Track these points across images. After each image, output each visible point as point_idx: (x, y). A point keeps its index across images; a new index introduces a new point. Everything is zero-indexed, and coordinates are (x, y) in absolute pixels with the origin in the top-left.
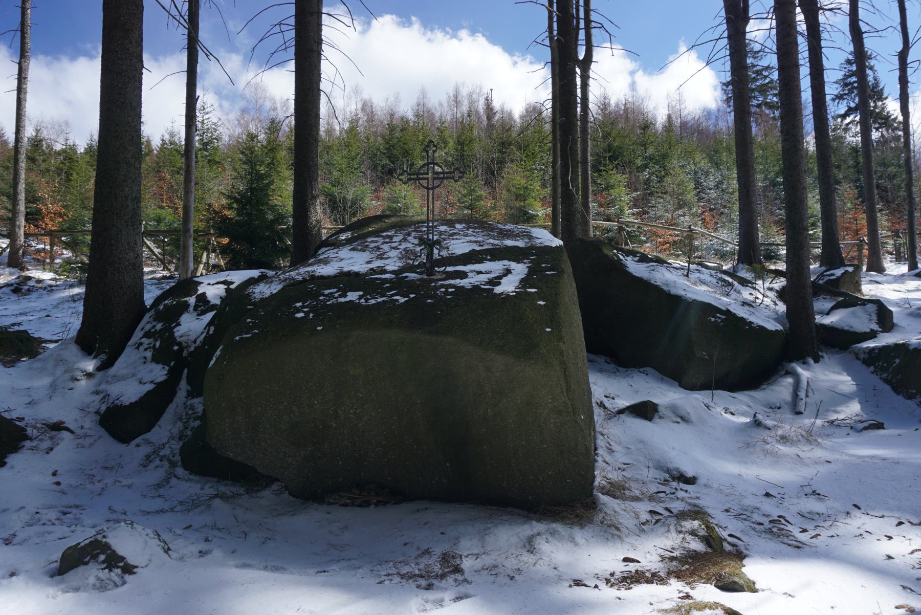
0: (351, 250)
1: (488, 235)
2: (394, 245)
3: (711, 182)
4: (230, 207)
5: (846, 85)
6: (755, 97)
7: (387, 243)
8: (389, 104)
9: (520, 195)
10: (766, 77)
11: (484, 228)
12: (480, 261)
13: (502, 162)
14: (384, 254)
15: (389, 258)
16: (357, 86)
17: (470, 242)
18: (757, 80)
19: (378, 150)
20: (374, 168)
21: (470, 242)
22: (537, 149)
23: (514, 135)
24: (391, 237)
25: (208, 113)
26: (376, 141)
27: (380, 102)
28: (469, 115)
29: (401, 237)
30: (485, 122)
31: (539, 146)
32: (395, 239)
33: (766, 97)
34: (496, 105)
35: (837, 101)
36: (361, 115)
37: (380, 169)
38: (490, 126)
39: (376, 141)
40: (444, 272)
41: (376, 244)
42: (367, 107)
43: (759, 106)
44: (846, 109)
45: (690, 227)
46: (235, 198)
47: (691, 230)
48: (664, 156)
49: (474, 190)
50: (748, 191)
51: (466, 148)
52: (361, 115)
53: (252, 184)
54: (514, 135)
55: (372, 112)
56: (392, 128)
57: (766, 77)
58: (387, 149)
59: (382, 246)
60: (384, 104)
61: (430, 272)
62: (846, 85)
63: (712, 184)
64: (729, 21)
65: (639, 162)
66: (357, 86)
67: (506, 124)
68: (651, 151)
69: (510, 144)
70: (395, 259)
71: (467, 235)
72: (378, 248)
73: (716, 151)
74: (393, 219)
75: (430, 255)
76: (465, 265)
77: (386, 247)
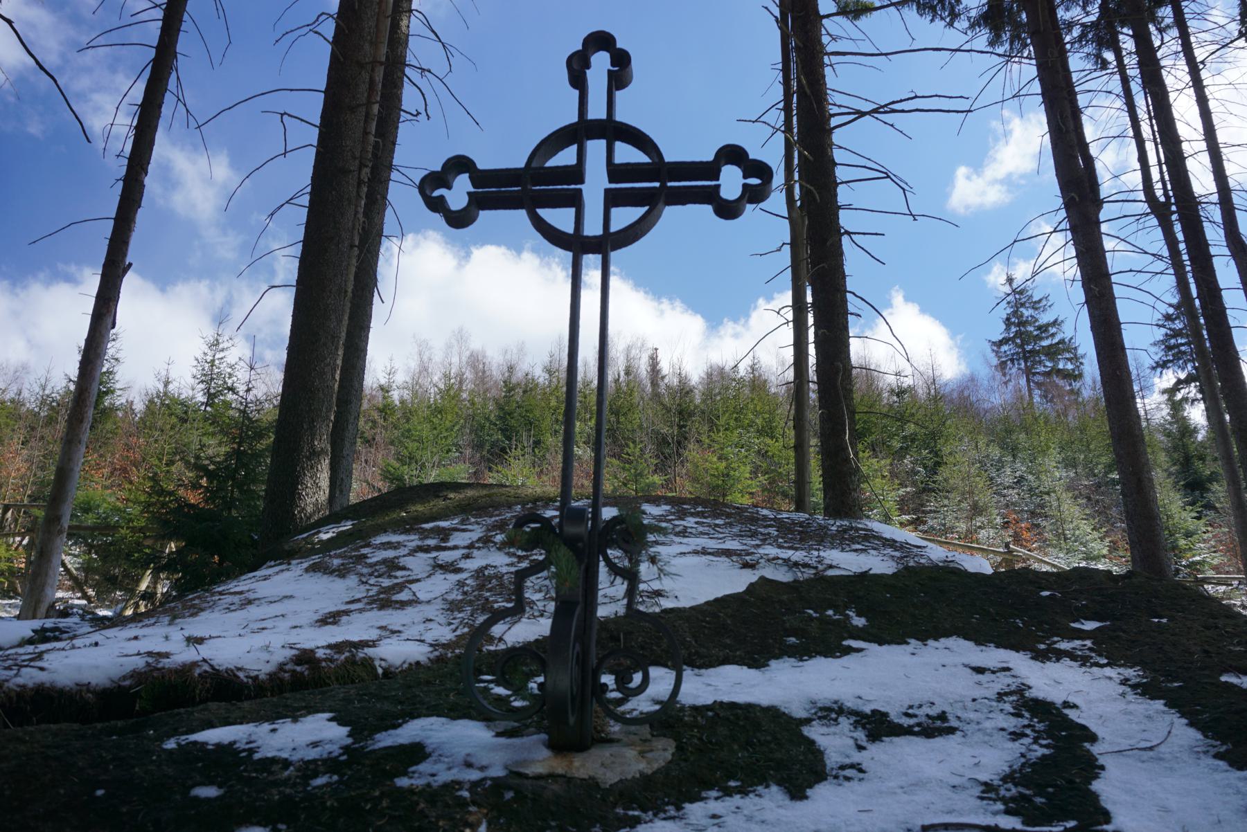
0: (307, 570)
1: (753, 535)
2: (445, 557)
3: (1007, 477)
4: (195, 486)
5: (1169, 348)
6: (1040, 362)
7: (427, 550)
8: (508, 357)
9: (718, 486)
10: (1053, 335)
11: (728, 516)
12: (827, 643)
13: (681, 442)
14: (400, 587)
15: (415, 602)
16: (460, 330)
17: (704, 552)
18: (1042, 339)
19: (487, 419)
20: (478, 446)
21: (704, 552)
22: (732, 423)
23: (698, 401)
24: (445, 534)
25: (222, 350)
26: (484, 406)
27: (495, 361)
28: (627, 373)
29: (476, 533)
30: (649, 388)
31: (736, 419)
32: (459, 539)
33: (1056, 362)
34: (665, 367)
35: (1159, 370)
36: (469, 375)
37: (487, 447)
38: (656, 396)
39: (484, 406)
40: (669, 719)
41: (390, 554)
42: (475, 361)
43: (1048, 374)
44: (1174, 380)
45: (1007, 545)
46: (204, 469)
47: (1010, 552)
48: (934, 436)
49: (641, 475)
50: (1140, 481)
51: (622, 419)
52: (469, 375)
53: (240, 444)
54: (698, 401)
55: (484, 372)
56: (509, 387)
57: (1053, 335)
58: (500, 418)
59: (408, 561)
60: (501, 358)
61: (571, 720)
62: (1169, 348)
63: (1009, 480)
64: (1068, 205)
65: (896, 444)
66: (460, 330)
67: (684, 390)
68: (911, 428)
69: (691, 414)
70: (431, 611)
71: (684, 533)
72: (392, 566)
73: (1009, 432)
74: (470, 493)
75: (575, 604)
76: (756, 659)
77: (418, 564)
